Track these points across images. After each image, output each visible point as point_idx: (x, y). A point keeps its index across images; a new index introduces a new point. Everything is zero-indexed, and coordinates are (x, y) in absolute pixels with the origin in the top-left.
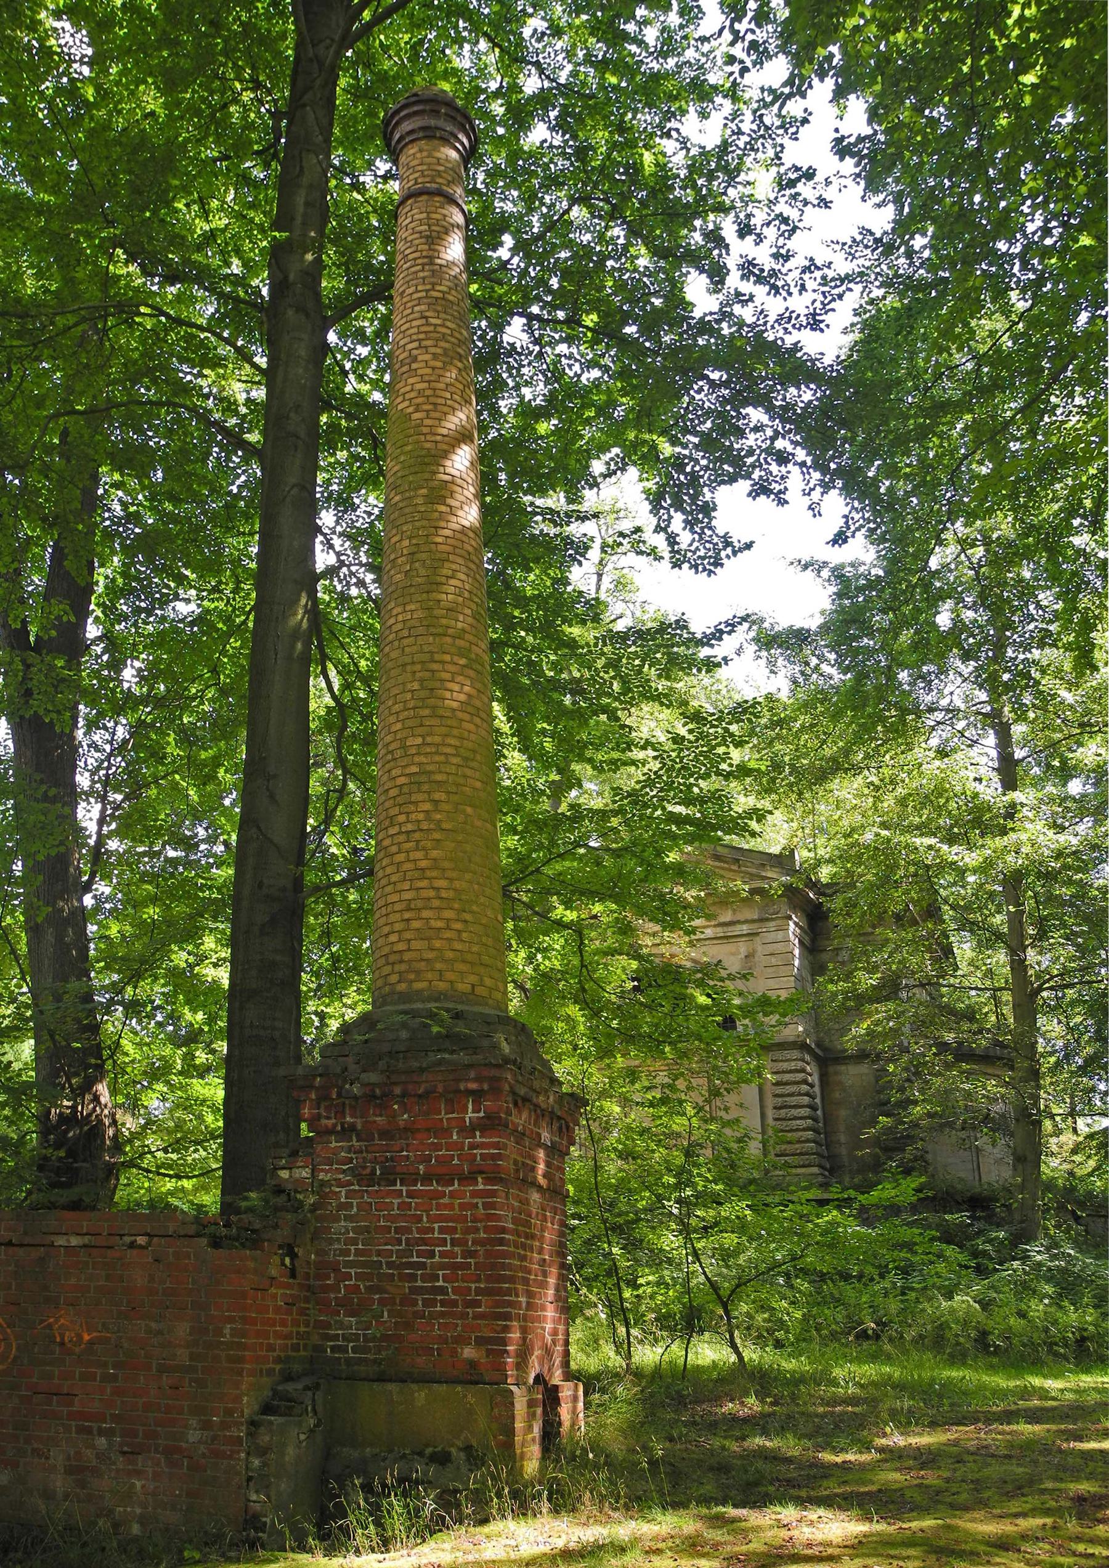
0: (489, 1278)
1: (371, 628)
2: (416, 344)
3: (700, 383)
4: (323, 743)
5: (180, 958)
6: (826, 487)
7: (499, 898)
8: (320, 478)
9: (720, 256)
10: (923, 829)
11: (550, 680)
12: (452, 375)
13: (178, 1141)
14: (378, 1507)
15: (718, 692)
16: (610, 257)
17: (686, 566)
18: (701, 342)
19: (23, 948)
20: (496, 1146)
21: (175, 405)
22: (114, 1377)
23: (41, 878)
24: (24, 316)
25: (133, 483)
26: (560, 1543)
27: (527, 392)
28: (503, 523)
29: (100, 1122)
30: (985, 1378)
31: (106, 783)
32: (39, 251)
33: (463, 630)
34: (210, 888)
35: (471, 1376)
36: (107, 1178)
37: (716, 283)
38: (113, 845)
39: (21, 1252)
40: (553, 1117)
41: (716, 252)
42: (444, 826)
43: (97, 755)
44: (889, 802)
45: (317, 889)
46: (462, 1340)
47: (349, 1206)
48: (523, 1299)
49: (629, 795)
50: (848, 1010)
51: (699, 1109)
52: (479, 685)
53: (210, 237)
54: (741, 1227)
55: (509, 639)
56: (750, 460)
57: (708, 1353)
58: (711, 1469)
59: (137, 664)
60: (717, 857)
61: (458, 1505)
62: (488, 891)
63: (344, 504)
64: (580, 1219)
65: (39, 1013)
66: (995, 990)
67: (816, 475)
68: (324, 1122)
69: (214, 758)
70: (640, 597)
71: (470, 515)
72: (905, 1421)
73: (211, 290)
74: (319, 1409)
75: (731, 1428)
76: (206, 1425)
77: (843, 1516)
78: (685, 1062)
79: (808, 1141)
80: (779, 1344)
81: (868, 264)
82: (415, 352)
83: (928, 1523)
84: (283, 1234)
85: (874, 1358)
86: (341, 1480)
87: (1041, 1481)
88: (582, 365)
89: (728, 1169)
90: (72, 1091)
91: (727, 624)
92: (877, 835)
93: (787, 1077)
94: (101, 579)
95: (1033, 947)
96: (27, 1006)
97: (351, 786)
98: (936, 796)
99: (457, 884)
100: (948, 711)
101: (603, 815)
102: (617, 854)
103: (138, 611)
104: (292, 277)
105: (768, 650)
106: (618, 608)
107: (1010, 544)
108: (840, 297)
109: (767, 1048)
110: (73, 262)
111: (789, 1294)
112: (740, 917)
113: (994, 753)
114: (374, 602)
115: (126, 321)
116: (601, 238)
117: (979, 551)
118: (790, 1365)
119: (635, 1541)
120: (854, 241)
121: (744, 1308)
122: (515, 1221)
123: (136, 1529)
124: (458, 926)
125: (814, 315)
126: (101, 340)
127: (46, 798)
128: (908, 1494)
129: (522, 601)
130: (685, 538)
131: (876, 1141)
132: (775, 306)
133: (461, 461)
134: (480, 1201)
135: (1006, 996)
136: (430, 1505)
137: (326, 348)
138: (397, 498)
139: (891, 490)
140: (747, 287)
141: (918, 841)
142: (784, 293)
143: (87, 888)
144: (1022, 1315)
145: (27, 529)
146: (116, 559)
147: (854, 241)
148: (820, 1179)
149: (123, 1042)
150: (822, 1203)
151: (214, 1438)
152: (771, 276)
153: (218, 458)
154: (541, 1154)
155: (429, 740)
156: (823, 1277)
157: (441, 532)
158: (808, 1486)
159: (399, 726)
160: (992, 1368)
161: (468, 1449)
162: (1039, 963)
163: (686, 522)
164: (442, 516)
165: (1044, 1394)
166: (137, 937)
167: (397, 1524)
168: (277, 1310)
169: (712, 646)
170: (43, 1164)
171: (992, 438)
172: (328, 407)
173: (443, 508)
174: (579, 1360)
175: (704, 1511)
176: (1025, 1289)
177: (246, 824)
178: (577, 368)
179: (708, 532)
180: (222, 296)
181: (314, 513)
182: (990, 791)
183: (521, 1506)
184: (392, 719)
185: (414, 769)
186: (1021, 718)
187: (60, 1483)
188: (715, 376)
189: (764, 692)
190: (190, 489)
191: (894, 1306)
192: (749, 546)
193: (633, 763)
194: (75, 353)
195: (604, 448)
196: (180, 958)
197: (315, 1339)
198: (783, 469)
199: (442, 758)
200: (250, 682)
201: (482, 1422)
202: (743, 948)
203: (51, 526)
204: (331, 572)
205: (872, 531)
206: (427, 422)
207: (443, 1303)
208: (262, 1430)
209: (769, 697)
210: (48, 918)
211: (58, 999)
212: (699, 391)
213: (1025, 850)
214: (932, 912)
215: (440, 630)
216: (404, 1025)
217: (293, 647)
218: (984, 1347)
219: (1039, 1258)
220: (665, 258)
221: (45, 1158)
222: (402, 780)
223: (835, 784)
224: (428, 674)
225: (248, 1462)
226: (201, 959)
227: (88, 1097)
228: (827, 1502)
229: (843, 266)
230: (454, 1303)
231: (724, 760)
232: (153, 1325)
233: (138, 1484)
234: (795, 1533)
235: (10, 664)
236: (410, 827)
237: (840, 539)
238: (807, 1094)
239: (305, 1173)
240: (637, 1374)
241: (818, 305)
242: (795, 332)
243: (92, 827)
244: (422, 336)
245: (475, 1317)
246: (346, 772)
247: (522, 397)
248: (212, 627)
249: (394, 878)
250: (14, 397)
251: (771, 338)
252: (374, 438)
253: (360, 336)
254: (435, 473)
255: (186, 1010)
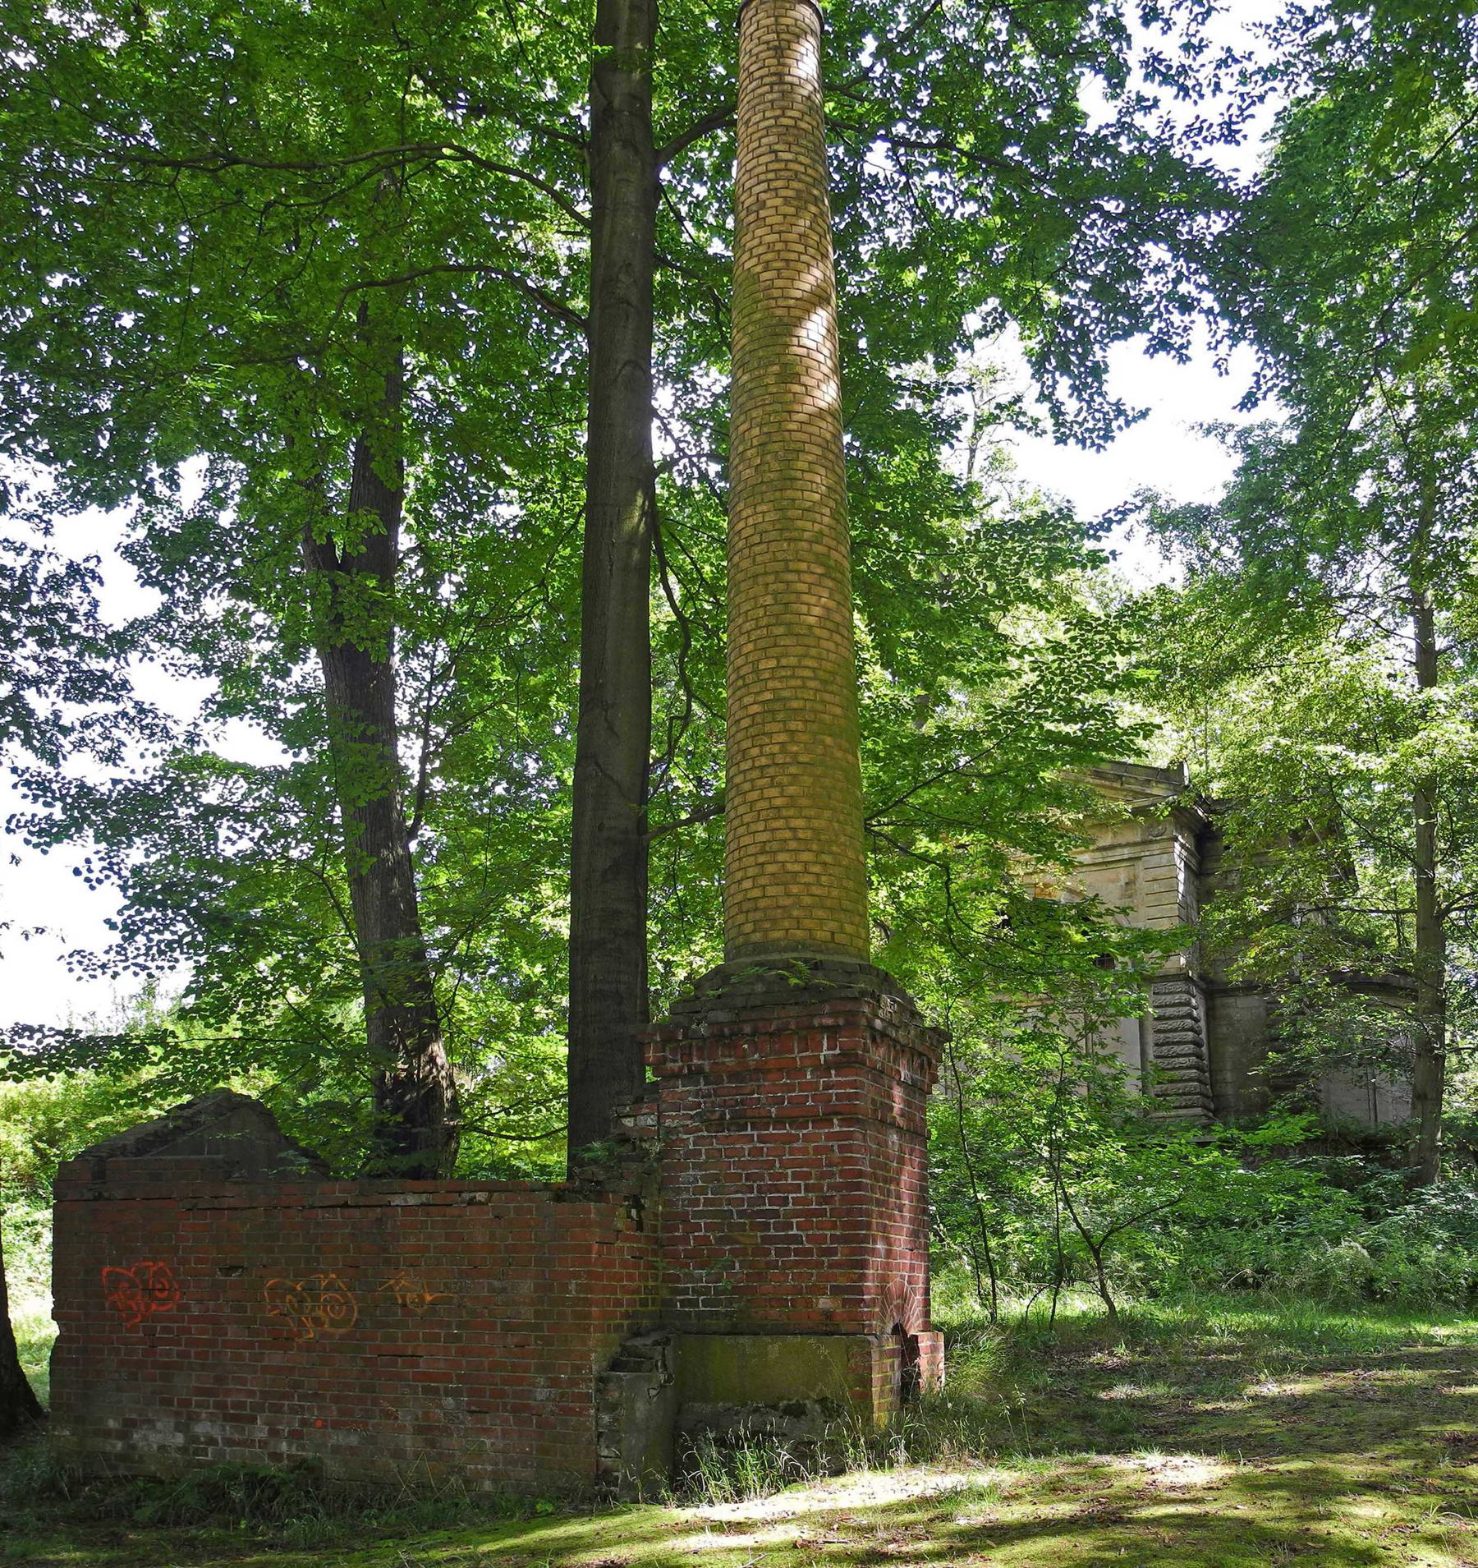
0: (845, 1225)
1: (719, 529)
2: (764, 186)
3: (1094, 216)
4: (665, 663)
5: (516, 906)
6: (1235, 338)
7: (861, 833)
8: (656, 348)
9: (1120, 50)
10: (1327, 736)
11: (916, 584)
12: (804, 223)
13: (520, 1101)
14: (732, 1459)
15: (1104, 584)
16: (989, 59)
17: (1072, 441)
18: (1095, 163)
19: (346, 900)
20: (853, 1084)
21: (488, 270)
22: (458, 1338)
23: (363, 826)
24: (310, 167)
25: (443, 365)
26: (917, 1491)
27: (891, 234)
28: (864, 393)
29: (437, 1084)
30: (1369, 1325)
31: (427, 718)
32: (323, 83)
33: (821, 533)
34: (545, 830)
35: (827, 1327)
36: (447, 1144)
37: (1115, 86)
38: (437, 784)
39: (357, 1213)
40: (913, 1053)
41: (1115, 46)
42: (802, 759)
43: (416, 684)
44: (1291, 704)
45: (663, 829)
46: (819, 1291)
47: (698, 1153)
48: (880, 1246)
49: (1004, 714)
50: (1236, 939)
51: (1073, 1044)
52: (837, 597)
53: (519, 51)
54: (1116, 1172)
55: (871, 538)
56: (1147, 309)
57: (1079, 1303)
58: (1076, 1417)
59: (456, 578)
60: (1098, 774)
61: (813, 1457)
62: (849, 829)
63: (680, 377)
64: (946, 1167)
65: (367, 973)
66: (1398, 912)
67: (1225, 324)
68: (670, 1065)
69: (547, 684)
70: (1016, 475)
71: (828, 394)
72: (1281, 1368)
73: (524, 123)
74: (670, 1363)
75: (1098, 1378)
76: (554, 1383)
77: (1210, 1460)
78: (1059, 996)
79: (1191, 1080)
80: (1153, 1294)
81: (1295, 50)
82: (763, 196)
83: (1297, 1465)
84: (628, 1185)
85: (1251, 1307)
86: (693, 1434)
87: (1417, 1424)
88: (956, 198)
89: (1104, 1102)
90: (407, 1052)
91: (1117, 512)
92: (1277, 744)
93: (1170, 1011)
94: (411, 481)
95: (1443, 862)
96: (356, 964)
97: (694, 706)
98: (1342, 697)
99: (816, 823)
100: (1362, 596)
101: (972, 736)
102: (988, 780)
103: (453, 516)
104: (617, 103)
105: (1162, 532)
106: (993, 489)
107: (1447, 400)
108: (1261, 98)
109: (1149, 980)
110: (363, 95)
111: (1165, 1241)
112: (1123, 841)
113: (1412, 645)
114: (719, 497)
115: (427, 167)
116: (979, 33)
117: (1410, 410)
118: (1164, 1315)
119: (994, 1488)
120: (1280, 22)
121: (1117, 1257)
122: (872, 1164)
123: (487, 1485)
124: (817, 869)
125: (1229, 123)
126: (399, 191)
127: (363, 738)
128: (1279, 1438)
129: (885, 492)
130: (1071, 406)
131: (1265, 1080)
132: (1182, 113)
133: (816, 330)
134: (835, 1144)
135: (1411, 918)
136: (785, 1455)
137: (658, 190)
138: (745, 378)
139: (1310, 338)
140: (1150, 90)
141: (1321, 748)
142: (1195, 96)
143: (412, 833)
144: (1413, 1260)
145: (329, 428)
146: (426, 456)
147: (1280, 22)
148: (1204, 1121)
149: (458, 999)
150: (1202, 1145)
151: (562, 1395)
152: (1179, 74)
153: (538, 331)
154: (897, 1092)
155: (784, 662)
156: (1203, 1223)
157: (796, 417)
158: (1175, 1434)
159: (751, 646)
160: (1377, 1316)
161: (822, 1401)
162: (1449, 881)
163: (1073, 387)
164: (797, 399)
165: (1429, 1341)
166: (470, 886)
167: (751, 1476)
168: (624, 1264)
169: (1099, 539)
170: (380, 1130)
171: (1432, 269)
172: (662, 263)
173: (797, 388)
174: (941, 1313)
175: (1067, 1458)
176: (1418, 1234)
177: (585, 760)
178: (949, 202)
179: (1098, 399)
180: (537, 131)
181: (649, 393)
182: (1406, 689)
183: (878, 1456)
184: (743, 640)
185: (768, 696)
186: (1445, 603)
187: (409, 1442)
188: (1110, 206)
189: (1156, 583)
190: (508, 370)
191: (1277, 1253)
192: (1144, 414)
193: (1009, 674)
194: (370, 209)
195: (979, 299)
196: (516, 906)
197: (665, 1294)
198: (1186, 318)
199: (799, 683)
200: (584, 597)
201: (837, 1372)
202: (1123, 874)
203: (354, 421)
204: (668, 464)
205: (1285, 391)
206: (779, 283)
207: (797, 1252)
208: (611, 1386)
209: (1161, 589)
210: (372, 870)
211: (388, 956)
212: (1091, 227)
213: (1439, 751)
214: (1334, 829)
215: (796, 534)
216: (760, 978)
217: (629, 556)
218: (1369, 1293)
219: (1434, 1201)
220: (1055, 56)
221: (382, 1123)
222: (756, 708)
223: (1231, 686)
224: (782, 586)
225: (597, 1419)
226: (537, 908)
227: (423, 1059)
228: (1194, 1448)
229: (1266, 56)
230: (809, 1252)
231: (1109, 671)
232: (496, 1283)
233: (488, 1442)
234: (1159, 1477)
235: (318, 585)
236: (764, 761)
237: (1249, 401)
238: (1191, 1029)
239: (651, 1121)
240: (1002, 1326)
241: (1234, 111)
242: (1205, 146)
243: (414, 767)
244: (771, 176)
245: (831, 1266)
246: (690, 695)
247: (885, 241)
248: (538, 532)
249: (746, 819)
250: (304, 267)
251: (1178, 155)
252: (716, 300)
253: (698, 174)
254: (788, 346)
255: (524, 963)
